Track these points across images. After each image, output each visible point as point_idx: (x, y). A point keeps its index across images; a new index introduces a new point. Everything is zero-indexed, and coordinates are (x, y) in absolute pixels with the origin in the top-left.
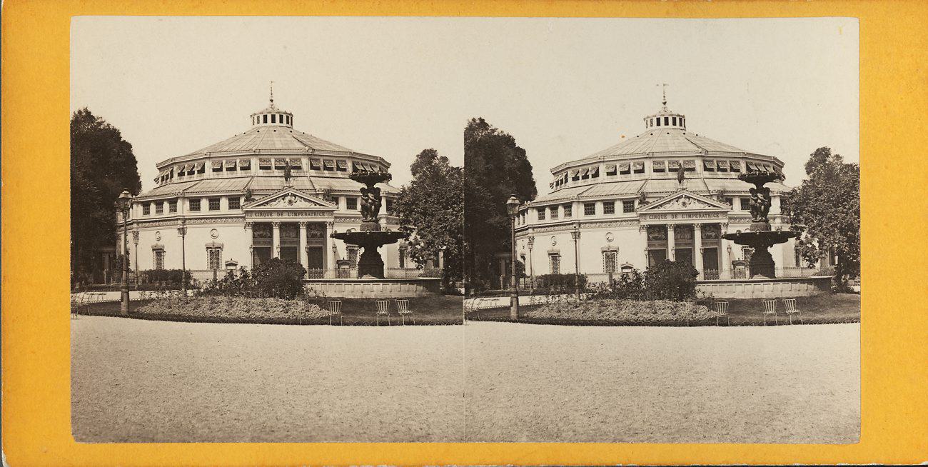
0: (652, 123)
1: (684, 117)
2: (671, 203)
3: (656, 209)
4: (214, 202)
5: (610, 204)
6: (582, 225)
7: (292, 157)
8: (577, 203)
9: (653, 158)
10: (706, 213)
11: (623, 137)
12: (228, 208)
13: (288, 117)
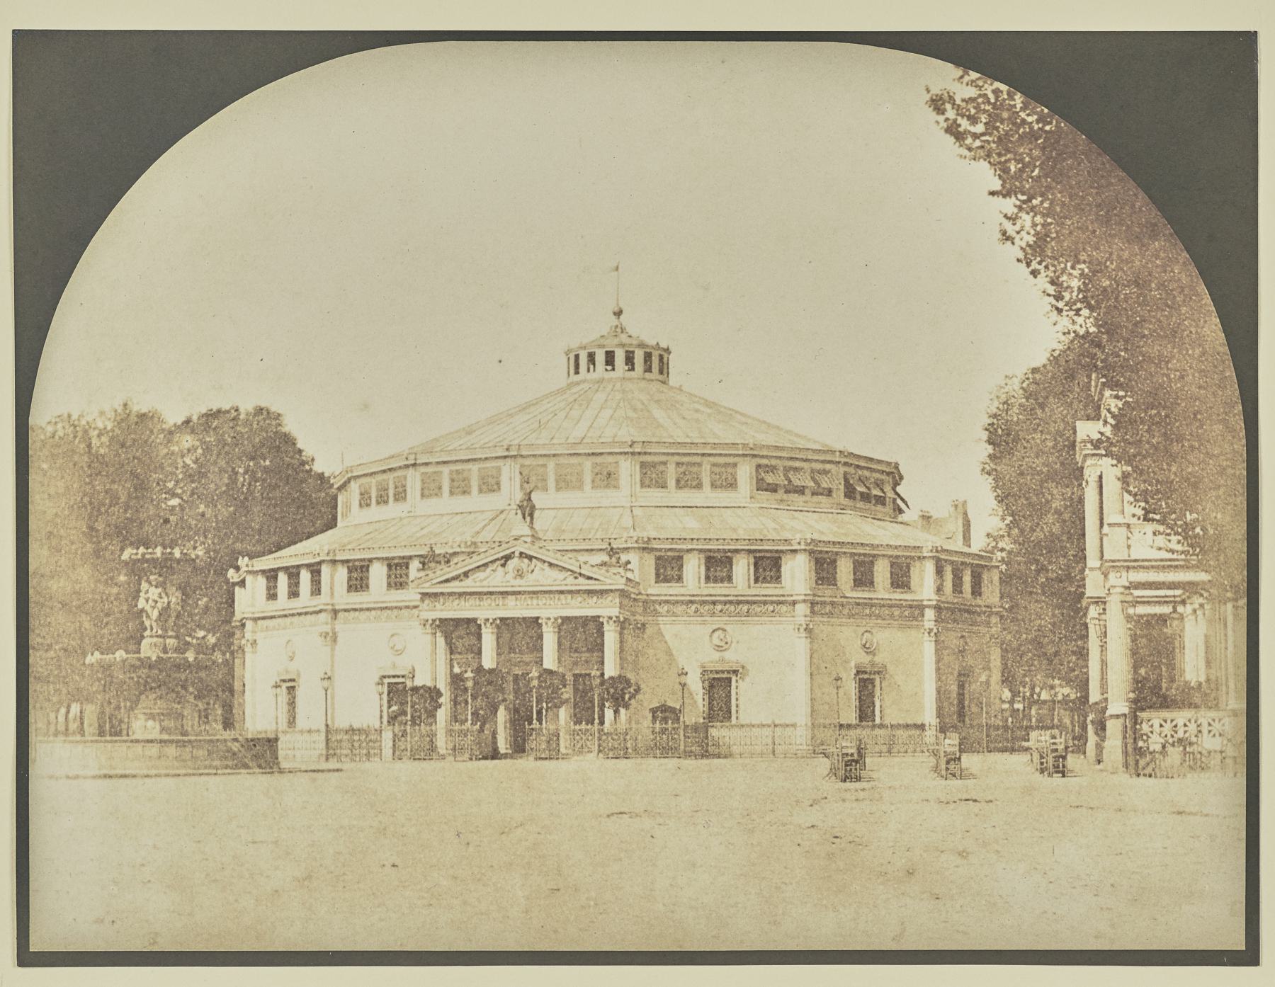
1: (667, 350)
3: (456, 583)
4: (718, 564)
6: (341, 615)
12: (385, 585)
13: (661, 357)
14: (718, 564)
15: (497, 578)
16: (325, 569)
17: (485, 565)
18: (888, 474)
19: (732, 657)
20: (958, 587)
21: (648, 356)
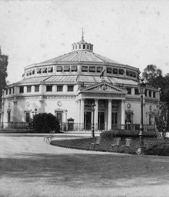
0: (76, 47)
2: (97, 88)
3: (90, 90)
5: (50, 86)
7: (120, 68)
8: (43, 85)
9: (82, 64)
10: (115, 94)
11: (86, 53)
13: (91, 46)
14: (60, 88)
15: (100, 90)
16: (15, 88)
17: (97, 87)
18: (136, 71)
19: (62, 108)
20: (150, 95)
21: (88, 46)
